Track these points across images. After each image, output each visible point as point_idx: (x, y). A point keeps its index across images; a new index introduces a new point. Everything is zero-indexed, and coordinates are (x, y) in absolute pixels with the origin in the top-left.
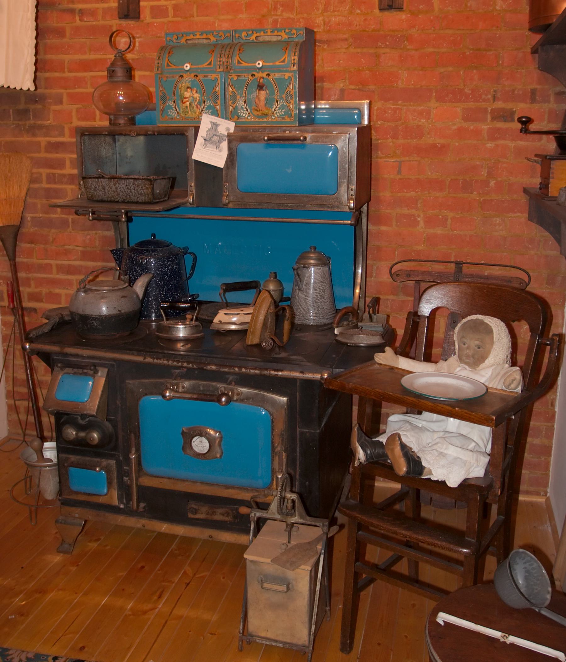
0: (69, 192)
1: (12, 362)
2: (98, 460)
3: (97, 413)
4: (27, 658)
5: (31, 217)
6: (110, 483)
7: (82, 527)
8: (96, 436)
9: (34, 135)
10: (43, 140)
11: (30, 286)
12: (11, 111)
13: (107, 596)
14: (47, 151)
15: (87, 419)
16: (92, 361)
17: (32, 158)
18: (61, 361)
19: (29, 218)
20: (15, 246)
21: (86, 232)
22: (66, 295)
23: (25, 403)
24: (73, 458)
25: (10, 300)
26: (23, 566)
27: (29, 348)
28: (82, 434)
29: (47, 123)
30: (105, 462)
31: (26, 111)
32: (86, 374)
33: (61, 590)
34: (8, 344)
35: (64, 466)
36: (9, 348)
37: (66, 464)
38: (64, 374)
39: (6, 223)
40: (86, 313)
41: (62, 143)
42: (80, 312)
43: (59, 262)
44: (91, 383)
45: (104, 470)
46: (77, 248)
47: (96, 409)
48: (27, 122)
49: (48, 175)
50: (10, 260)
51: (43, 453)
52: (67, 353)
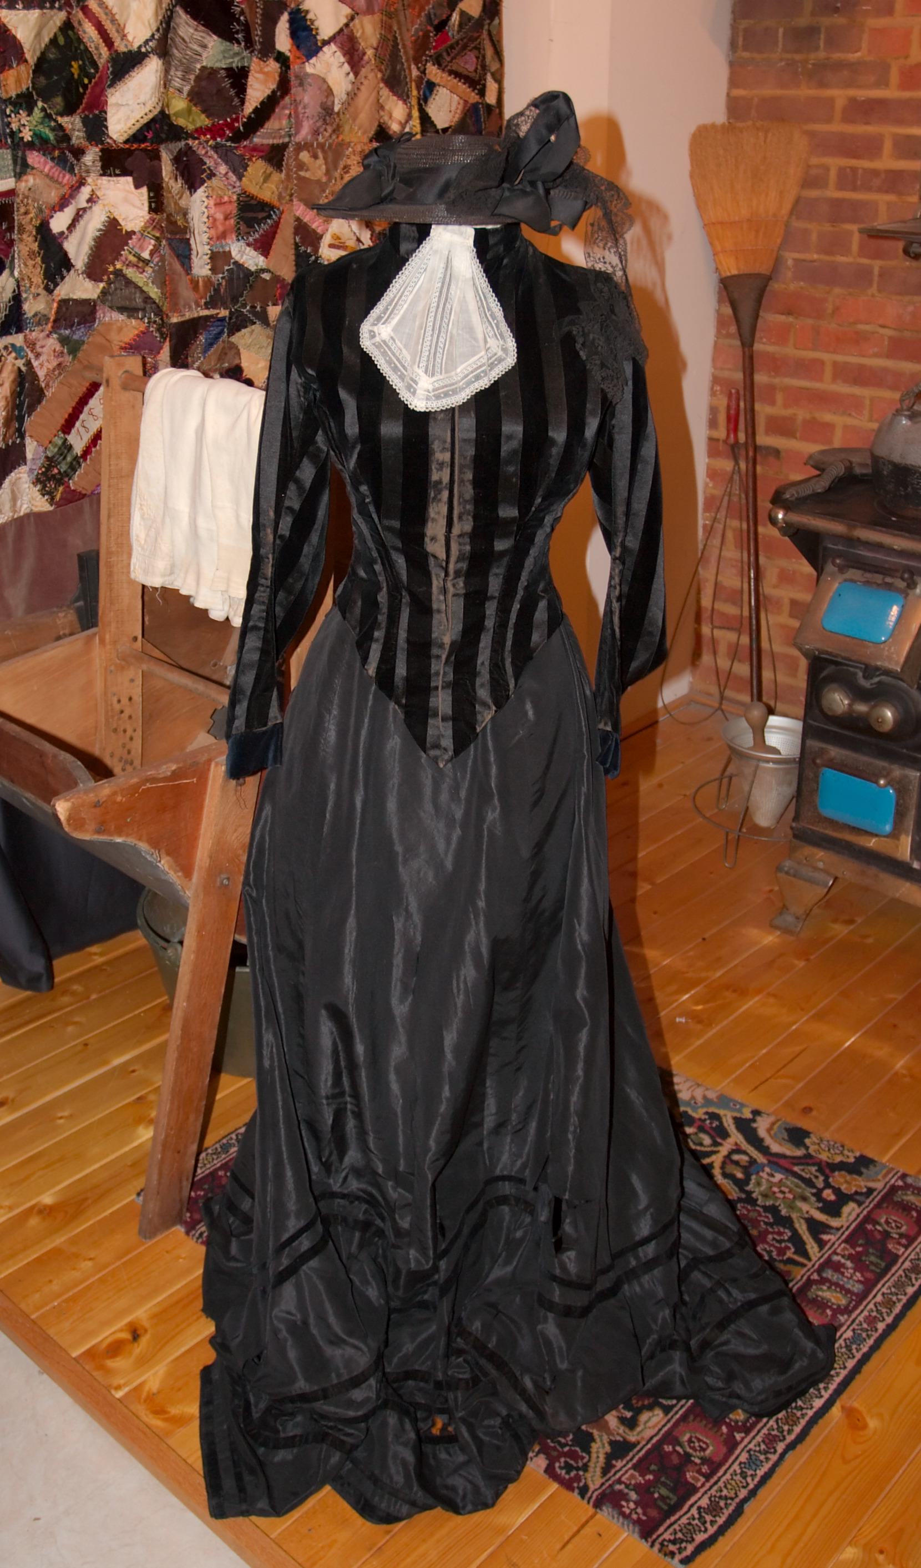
0: (883, 208)
1: (718, 552)
2: (885, 764)
3: (902, 669)
4: (705, 1097)
5: (794, 260)
6: (900, 815)
7: (826, 890)
8: (889, 714)
9: (822, 85)
10: (840, 95)
11: (773, 403)
12: (781, 31)
13: (854, 1034)
14: (847, 119)
15: (876, 680)
16: (904, 562)
17: (811, 135)
18: (840, 554)
19: (790, 262)
20: (756, 317)
21: (907, 298)
22: (846, 427)
23: (731, 636)
24: (835, 752)
25: (732, 426)
26: (706, 936)
27: (783, 519)
28: (862, 708)
29: (854, 57)
30: (897, 772)
31: (812, 31)
32: (889, 587)
33: (774, 996)
34: (713, 514)
35: (814, 762)
36: (716, 525)
37: (818, 761)
38: (846, 580)
39: (745, 269)
40: (908, 462)
41: (882, 102)
42: (896, 458)
43: (840, 358)
44: (895, 610)
45: (892, 786)
46: (882, 331)
47: (902, 660)
48: (813, 56)
49: (841, 171)
50: (743, 344)
51: (766, 735)
52: (859, 539)
